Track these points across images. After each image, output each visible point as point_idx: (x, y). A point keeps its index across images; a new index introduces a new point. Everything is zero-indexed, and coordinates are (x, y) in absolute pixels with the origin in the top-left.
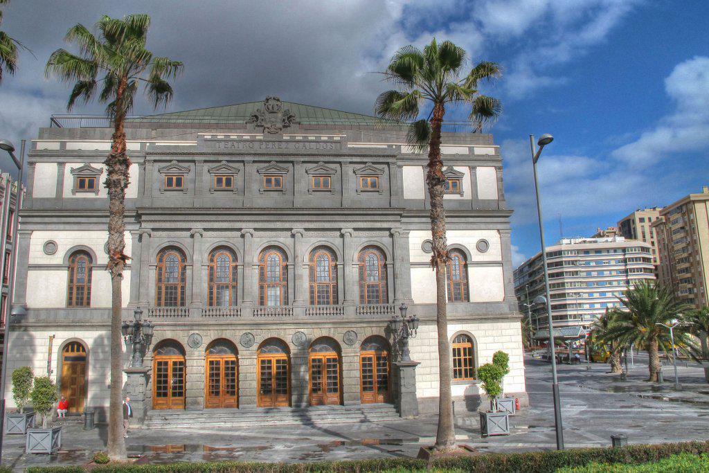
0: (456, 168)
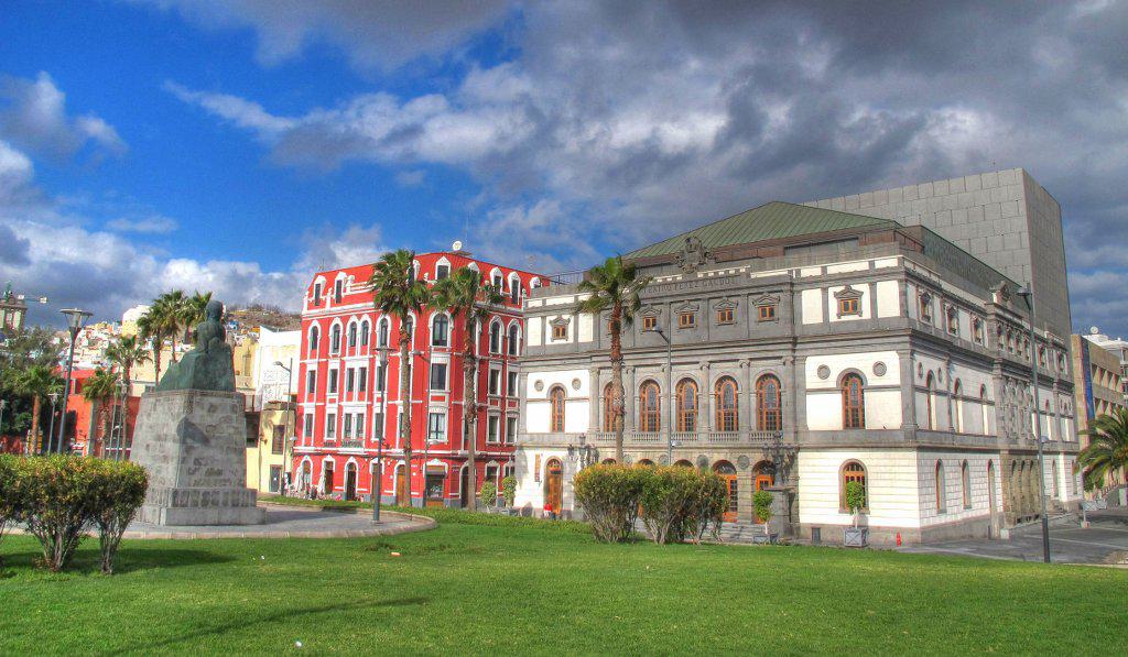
0: (855, 287)
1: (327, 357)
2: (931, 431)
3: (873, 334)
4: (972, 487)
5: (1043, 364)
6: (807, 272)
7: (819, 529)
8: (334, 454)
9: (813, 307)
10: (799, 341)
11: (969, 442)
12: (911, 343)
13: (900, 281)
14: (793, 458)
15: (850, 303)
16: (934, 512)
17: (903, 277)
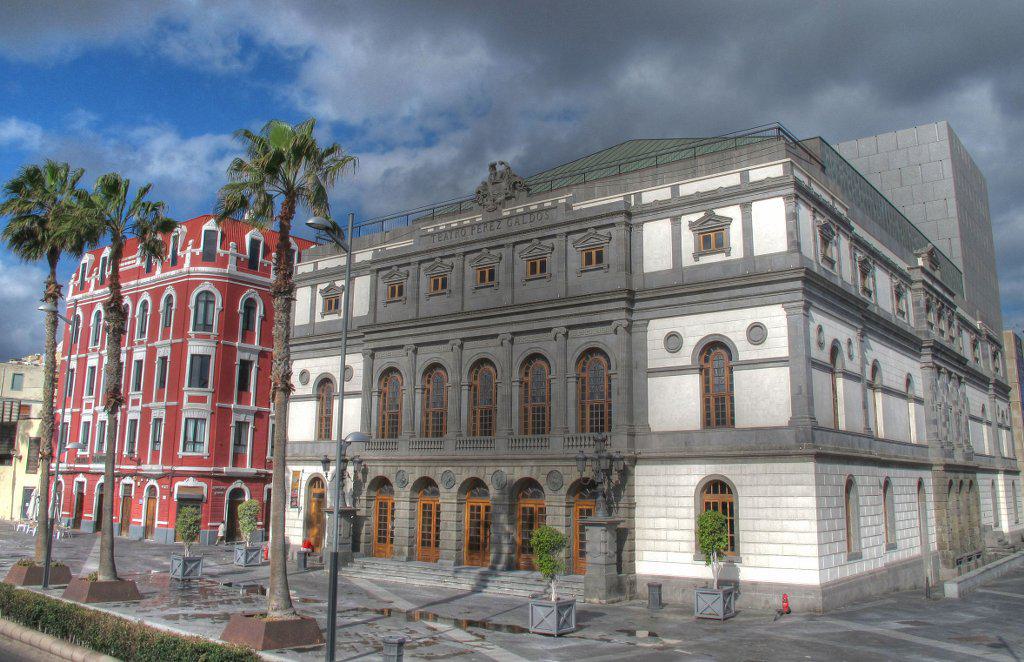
0: (719, 212)
1: (87, 351)
2: (836, 430)
3: (749, 282)
4: (897, 516)
5: (977, 360)
6: (649, 196)
7: (660, 586)
8: (86, 472)
9: (659, 246)
10: (641, 297)
11: (892, 452)
12: (805, 292)
13: (786, 197)
14: (626, 474)
15: (712, 236)
16: (843, 557)
17: (791, 190)
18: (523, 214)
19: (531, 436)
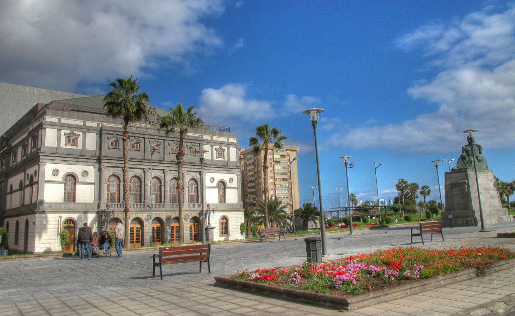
3: (81, 157)
15: (221, 153)
18: (143, 128)
19: (159, 204)
